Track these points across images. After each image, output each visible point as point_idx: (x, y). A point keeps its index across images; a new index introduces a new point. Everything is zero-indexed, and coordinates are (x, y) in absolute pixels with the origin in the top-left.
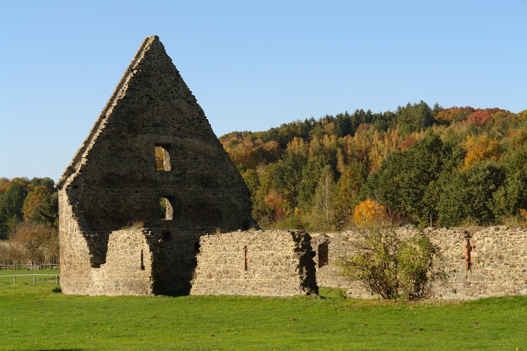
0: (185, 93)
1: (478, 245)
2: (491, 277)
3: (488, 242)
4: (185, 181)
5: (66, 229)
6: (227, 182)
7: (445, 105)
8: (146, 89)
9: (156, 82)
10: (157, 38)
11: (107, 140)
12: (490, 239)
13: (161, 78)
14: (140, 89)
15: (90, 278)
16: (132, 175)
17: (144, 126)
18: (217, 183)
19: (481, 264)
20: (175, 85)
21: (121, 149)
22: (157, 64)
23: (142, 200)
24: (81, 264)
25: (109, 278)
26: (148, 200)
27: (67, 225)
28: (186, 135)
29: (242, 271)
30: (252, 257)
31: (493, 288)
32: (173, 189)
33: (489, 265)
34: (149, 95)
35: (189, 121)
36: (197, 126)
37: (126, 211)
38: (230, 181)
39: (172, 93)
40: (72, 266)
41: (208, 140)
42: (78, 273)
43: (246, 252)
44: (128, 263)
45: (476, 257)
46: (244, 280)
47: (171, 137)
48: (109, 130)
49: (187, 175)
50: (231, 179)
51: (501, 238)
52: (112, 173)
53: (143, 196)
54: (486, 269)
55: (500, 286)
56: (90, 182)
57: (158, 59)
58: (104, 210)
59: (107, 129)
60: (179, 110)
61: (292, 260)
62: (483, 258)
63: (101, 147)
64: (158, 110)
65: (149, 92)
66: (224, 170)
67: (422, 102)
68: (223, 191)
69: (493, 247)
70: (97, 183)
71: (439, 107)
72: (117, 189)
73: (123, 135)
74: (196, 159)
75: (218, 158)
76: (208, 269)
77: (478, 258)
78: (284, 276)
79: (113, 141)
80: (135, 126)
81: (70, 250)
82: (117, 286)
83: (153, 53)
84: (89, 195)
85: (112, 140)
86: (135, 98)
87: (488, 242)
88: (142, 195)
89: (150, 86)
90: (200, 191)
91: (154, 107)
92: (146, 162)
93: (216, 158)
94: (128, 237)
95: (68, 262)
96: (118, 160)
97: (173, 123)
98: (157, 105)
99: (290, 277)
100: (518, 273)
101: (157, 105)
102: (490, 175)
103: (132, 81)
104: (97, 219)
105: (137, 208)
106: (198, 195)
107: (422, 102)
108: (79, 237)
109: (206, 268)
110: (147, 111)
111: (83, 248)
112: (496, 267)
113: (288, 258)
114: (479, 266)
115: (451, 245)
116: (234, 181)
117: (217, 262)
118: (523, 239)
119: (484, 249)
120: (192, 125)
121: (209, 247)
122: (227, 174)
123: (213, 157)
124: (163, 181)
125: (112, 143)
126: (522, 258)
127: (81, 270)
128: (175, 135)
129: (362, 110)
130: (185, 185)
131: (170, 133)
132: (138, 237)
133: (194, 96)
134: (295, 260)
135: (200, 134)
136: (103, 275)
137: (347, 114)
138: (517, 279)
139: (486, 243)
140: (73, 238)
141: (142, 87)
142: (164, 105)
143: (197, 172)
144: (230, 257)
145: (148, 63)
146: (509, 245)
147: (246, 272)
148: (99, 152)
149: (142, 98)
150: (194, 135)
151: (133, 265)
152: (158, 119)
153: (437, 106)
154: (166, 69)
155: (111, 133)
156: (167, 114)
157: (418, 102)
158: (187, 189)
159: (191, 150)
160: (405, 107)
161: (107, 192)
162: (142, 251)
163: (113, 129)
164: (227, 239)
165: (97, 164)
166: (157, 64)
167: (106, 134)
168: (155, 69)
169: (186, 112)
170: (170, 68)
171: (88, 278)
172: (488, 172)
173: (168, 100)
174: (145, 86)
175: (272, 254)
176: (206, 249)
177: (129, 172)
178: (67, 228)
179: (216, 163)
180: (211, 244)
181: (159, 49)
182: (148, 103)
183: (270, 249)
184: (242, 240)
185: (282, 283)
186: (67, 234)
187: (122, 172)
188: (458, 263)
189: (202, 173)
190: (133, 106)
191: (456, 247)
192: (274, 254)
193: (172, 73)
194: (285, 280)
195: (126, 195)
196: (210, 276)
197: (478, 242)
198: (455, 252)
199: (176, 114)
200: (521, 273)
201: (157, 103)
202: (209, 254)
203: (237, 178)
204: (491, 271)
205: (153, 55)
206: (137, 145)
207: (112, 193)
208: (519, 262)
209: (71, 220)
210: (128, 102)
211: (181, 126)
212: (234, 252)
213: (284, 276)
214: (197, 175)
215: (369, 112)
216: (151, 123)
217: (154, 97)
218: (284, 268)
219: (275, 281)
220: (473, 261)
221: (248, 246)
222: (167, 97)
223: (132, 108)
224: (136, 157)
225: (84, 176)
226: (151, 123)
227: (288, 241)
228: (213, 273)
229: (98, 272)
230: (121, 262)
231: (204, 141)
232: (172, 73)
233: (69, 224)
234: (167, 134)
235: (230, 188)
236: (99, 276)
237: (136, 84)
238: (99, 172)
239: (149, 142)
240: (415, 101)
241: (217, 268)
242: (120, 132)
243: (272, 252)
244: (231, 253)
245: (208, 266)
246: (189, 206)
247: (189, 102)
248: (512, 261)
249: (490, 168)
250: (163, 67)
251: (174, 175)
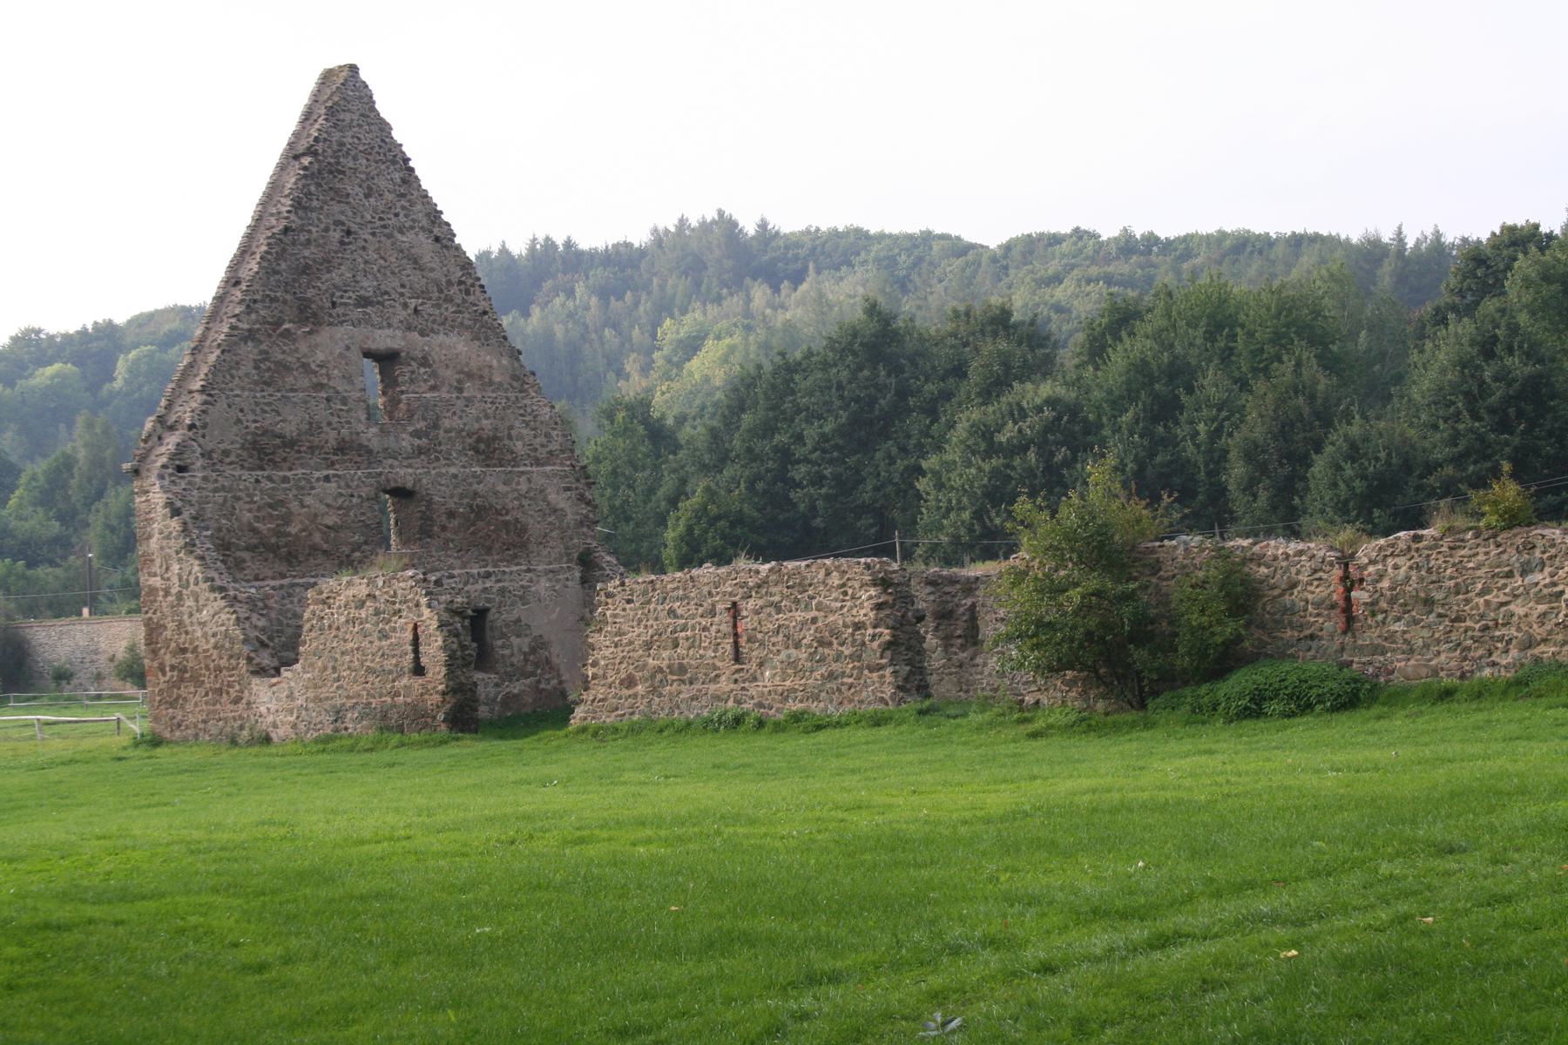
0: (428, 215)
1: (1369, 575)
2: (1405, 647)
3: (1396, 567)
4: (439, 448)
5: (163, 579)
6: (536, 450)
7: (788, 223)
8: (336, 208)
9: (357, 189)
10: (353, 69)
11: (250, 344)
12: (1400, 561)
13: (369, 177)
14: (322, 208)
15: (249, 703)
16: (312, 435)
17: (334, 304)
18: (512, 453)
19: (1380, 617)
20: (403, 195)
21: (284, 368)
22: (359, 139)
23: (340, 501)
24: (219, 669)
25: (313, 701)
26: (355, 500)
27: (167, 569)
28: (435, 326)
29: (727, 666)
30: (755, 629)
31: (1410, 670)
32: (410, 470)
33: (1398, 619)
34: (343, 224)
35: (441, 291)
36: (459, 301)
37: (304, 530)
38: (542, 446)
39: (397, 215)
40: (187, 675)
41: (487, 339)
42: (207, 694)
43: (735, 617)
44: (372, 661)
45: (1365, 604)
46: (732, 686)
47: (399, 333)
48: (253, 316)
49: (441, 432)
50: (544, 440)
51: (1428, 556)
52: (265, 432)
53: (343, 491)
54: (1392, 628)
55: (1426, 666)
56: (215, 456)
57: (360, 126)
58: (254, 530)
59: (249, 314)
60: (416, 262)
61: (870, 631)
62: (1383, 605)
63: (237, 363)
64: (366, 262)
65: (342, 213)
66: (528, 418)
67: (721, 213)
68: (528, 472)
69: (1408, 578)
70: (233, 458)
71: (770, 227)
72: (281, 474)
73: (286, 330)
74: (460, 390)
75: (512, 386)
76: (623, 666)
77: (1373, 604)
78: (848, 671)
79: (263, 347)
80: (313, 306)
81: (180, 634)
82: (336, 721)
83: (349, 111)
84: (215, 490)
85: (261, 342)
86: (310, 232)
87: (1396, 567)
88: (339, 487)
89: (341, 197)
90: (474, 475)
91: (355, 255)
92: (344, 401)
93: (506, 386)
94: (369, 595)
95: (173, 668)
96: (279, 394)
97: (402, 295)
98: (364, 248)
99: (866, 672)
100: (1470, 633)
101: (364, 248)
102: (1053, 422)
103: (300, 186)
104: (239, 554)
105: (330, 521)
106: (471, 484)
107: (721, 213)
108: (208, 599)
109: (618, 661)
110: (340, 264)
111: (224, 628)
112: (1416, 622)
113: (858, 626)
114: (1373, 624)
115: (1303, 578)
116: (554, 446)
117: (648, 645)
118: (1481, 557)
119: (1385, 584)
120: (449, 300)
121: (624, 610)
122: (534, 429)
123: (500, 384)
124: (385, 450)
125: (261, 352)
126: (1481, 601)
127: (218, 686)
128: (409, 328)
129: (547, 239)
130: (437, 459)
131: (395, 321)
132: (400, 592)
133: (448, 224)
134: (878, 630)
135: (467, 322)
136: (290, 696)
137: (504, 251)
138: (1469, 649)
139: (1390, 570)
140: (190, 603)
141: (325, 202)
142: (379, 249)
143: (465, 424)
144: (689, 633)
145: (336, 136)
146: (1449, 571)
147: (737, 667)
148: (232, 377)
149: (327, 230)
150: (452, 327)
151: (389, 664)
152: (367, 286)
153: (763, 225)
154: (379, 153)
155: (257, 326)
156: (388, 273)
157: (711, 215)
158: (443, 471)
159: (447, 366)
160: (673, 229)
161: (257, 481)
162: (415, 627)
163: (262, 312)
164: (678, 588)
165: (229, 406)
166: (359, 139)
167: (246, 326)
168: (353, 153)
169: (433, 265)
170: (390, 150)
171: (241, 706)
172: (1048, 413)
173: (389, 236)
174: (332, 199)
175: (814, 620)
176: (615, 616)
177: (307, 427)
178: (168, 579)
179: (508, 399)
180: (629, 602)
181: (360, 98)
182: (342, 243)
183: (807, 607)
184: (722, 589)
185: (843, 688)
186: (167, 593)
187: (290, 429)
188: (1321, 620)
189: (476, 426)
190: (307, 253)
191: (1316, 583)
192: (820, 620)
193: (394, 162)
194: (850, 680)
195: (302, 488)
196: (630, 682)
197: (1371, 569)
198: (1313, 593)
199: (409, 272)
200: (1477, 634)
201: (363, 244)
202: (625, 628)
203: (560, 439)
204: (1404, 632)
205: (347, 116)
206: (320, 356)
207: (271, 485)
208: (1472, 609)
209: (181, 555)
210: (294, 243)
211: (422, 304)
212: (698, 619)
213: (848, 671)
214: (464, 434)
215: (568, 244)
216: (350, 298)
217: (354, 228)
218: (847, 652)
219: (823, 684)
220: (1358, 611)
221: (742, 605)
222: (385, 227)
223: (304, 258)
224: (319, 387)
225: (201, 440)
226: (350, 298)
227: (857, 585)
228: (638, 675)
229: (274, 688)
230: (347, 658)
231: (477, 343)
232: (394, 162)
233: (176, 568)
234: (389, 326)
235: (543, 465)
236: (279, 700)
237: (311, 194)
238: (235, 429)
239: (348, 348)
240: (699, 212)
241: (650, 661)
242: (278, 323)
243: (814, 613)
244: (691, 622)
245: (624, 657)
246: (451, 515)
247: (437, 239)
248: (1455, 608)
249: (1052, 402)
250: (372, 148)
251: (412, 434)
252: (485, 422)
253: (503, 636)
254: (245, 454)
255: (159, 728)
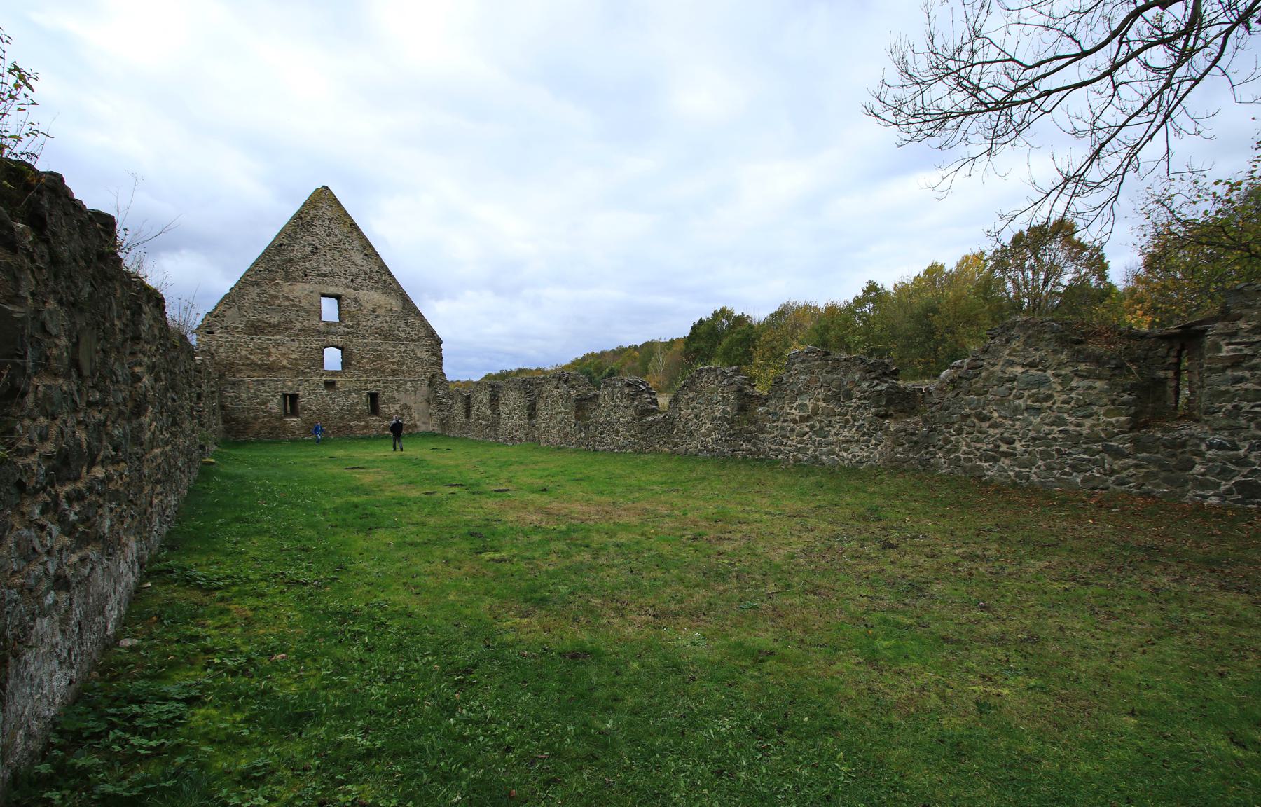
39: (344, 244)
70: (239, 330)
84: (226, 342)
128: (348, 287)
152: (325, 269)
189: (380, 325)
217: (319, 246)
252: (385, 324)
253: (384, 403)
254: (247, 329)
255: (881, 420)
